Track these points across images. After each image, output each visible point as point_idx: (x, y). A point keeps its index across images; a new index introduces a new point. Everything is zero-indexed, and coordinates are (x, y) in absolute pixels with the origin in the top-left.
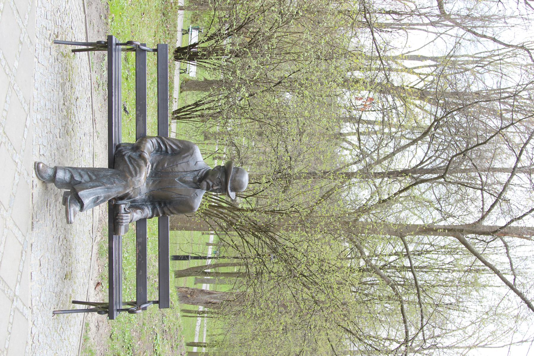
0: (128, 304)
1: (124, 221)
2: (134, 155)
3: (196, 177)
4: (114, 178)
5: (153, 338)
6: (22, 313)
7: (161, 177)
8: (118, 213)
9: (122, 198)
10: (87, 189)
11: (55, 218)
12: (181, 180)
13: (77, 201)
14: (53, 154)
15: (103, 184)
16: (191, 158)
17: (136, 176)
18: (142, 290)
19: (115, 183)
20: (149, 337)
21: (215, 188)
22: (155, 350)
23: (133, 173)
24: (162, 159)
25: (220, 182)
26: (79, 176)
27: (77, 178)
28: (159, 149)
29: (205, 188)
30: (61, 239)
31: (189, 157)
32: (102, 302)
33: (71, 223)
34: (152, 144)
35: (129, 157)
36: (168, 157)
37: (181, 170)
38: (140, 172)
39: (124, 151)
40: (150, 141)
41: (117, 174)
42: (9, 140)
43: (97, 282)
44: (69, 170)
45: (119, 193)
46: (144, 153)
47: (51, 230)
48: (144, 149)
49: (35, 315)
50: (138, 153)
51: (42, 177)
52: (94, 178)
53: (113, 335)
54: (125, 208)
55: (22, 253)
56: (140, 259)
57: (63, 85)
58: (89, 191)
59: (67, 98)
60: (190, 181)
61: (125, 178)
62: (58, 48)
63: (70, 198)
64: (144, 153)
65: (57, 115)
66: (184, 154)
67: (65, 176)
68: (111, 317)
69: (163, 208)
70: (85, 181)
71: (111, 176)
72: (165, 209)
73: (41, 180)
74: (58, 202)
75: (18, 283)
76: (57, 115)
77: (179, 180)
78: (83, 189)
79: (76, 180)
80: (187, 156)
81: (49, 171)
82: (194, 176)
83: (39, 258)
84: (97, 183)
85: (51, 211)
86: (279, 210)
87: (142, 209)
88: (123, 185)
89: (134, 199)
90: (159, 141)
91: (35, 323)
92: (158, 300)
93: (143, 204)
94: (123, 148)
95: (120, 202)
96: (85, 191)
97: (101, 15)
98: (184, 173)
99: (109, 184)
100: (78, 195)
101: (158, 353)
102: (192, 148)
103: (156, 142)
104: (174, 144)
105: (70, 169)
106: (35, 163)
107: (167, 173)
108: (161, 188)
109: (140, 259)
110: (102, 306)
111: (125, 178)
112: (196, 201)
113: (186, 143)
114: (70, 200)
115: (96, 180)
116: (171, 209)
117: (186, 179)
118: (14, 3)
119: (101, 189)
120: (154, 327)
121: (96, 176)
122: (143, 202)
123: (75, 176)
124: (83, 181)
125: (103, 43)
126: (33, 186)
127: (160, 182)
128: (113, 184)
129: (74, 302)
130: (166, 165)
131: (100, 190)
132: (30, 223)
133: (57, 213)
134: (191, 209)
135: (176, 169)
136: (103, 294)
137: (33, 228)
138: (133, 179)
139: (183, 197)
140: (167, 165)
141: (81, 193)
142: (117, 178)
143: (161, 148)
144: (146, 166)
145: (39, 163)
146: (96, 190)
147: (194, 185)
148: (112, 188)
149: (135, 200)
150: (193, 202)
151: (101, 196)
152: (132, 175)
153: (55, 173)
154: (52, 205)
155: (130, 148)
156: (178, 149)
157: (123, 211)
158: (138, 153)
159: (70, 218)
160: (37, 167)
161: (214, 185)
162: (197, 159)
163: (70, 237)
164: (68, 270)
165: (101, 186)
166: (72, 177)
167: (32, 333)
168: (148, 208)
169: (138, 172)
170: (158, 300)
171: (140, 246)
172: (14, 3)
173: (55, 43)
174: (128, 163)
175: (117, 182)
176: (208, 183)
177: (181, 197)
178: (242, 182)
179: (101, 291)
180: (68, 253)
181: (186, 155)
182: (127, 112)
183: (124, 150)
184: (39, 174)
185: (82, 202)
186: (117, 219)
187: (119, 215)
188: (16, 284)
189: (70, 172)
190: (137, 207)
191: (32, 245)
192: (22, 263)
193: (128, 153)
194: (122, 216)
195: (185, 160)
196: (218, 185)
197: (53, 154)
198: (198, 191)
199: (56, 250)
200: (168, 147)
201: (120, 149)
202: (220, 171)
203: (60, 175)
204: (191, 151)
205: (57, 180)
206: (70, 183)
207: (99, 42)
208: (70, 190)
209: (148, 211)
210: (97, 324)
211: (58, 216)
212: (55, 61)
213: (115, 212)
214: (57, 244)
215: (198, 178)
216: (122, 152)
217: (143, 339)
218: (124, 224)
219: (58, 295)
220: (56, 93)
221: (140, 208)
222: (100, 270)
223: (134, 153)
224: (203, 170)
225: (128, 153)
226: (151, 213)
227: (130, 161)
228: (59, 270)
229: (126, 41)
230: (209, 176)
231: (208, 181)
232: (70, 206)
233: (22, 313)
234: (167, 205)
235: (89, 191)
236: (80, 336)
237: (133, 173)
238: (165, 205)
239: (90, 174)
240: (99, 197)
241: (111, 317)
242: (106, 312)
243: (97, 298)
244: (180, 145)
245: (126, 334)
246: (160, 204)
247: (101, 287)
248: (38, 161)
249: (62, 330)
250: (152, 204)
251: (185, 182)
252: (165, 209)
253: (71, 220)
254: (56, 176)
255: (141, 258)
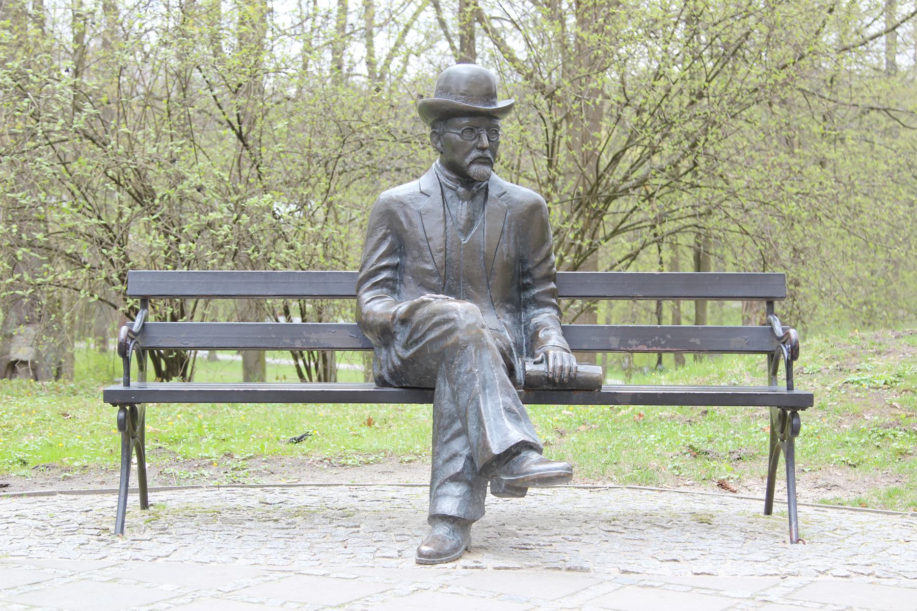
0: (774, 372)
1: (567, 365)
2: (401, 336)
3: (458, 195)
4: (459, 373)
5: (857, 390)
6: (796, 589)
7: (458, 280)
8: (548, 379)
9: (511, 371)
10: (484, 435)
11: (558, 538)
12: (466, 231)
13: (515, 459)
14: (398, 538)
15: (474, 399)
16: (412, 206)
17: (453, 320)
18: (739, 339)
19: (471, 371)
20: (853, 397)
21: (486, 143)
22: (886, 386)
23: (445, 327)
24: (413, 277)
25: (472, 130)
26: (454, 463)
27: (459, 465)
28: (388, 287)
29: (487, 169)
30: (611, 528)
31: (408, 211)
32: (766, 481)
33: (570, 469)
34: (377, 301)
35: (406, 346)
36: (409, 263)
37: (441, 229)
38: (444, 312)
39: (393, 363)
40: (369, 304)
41: (447, 368)
42: (359, 600)
43: (717, 489)
44: (438, 487)
45: (496, 361)
46: (398, 313)
47: (587, 544)
48: (388, 314)
49: (802, 570)
50: (398, 328)
51: (455, 549)
52: (457, 426)
53: (850, 462)
54: (535, 363)
55: (645, 586)
56: (663, 342)
57: (225, 520)
58: (491, 431)
59: (261, 516)
60: (468, 207)
61: (458, 347)
62: (135, 529)
63: (507, 476)
64: (398, 313)
65: (302, 532)
66: (401, 223)
67: (452, 496)
68: (806, 401)
69: (534, 279)
70: (465, 447)
71: (452, 381)
72: (539, 273)
73: (463, 553)
74: (518, 532)
75: (721, 593)
76: (302, 532)
77: (466, 235)
78: (485, 442)
79: (463, 469)
80: (406, 216)
81: (441, 532)
82: (456, 199)
83: (658, 563)
84: (471, 415)
85: (542, 543)
86: (547, 145)
87: (537, 327)
88: (476, 351)
89: (512, 345)
90: (368, 284)
91: (822, 570)
92: (764, 357)
93: (526, 328)
94: (385, 370)
95: (520, 376)
96: (489, 439)
97: (61, 477)
98: (449, 224)
99: (474, 385)
100: (499, 456)
101: (893, 378)
102: (386, 205)
103: (372, 292)
104: (376, 248)
105: (437, 484)
106: (419, 563)
107: (447, 262)
108: (485, 280)
109: (663, 342)
110: (779, 434)
111: (458, 347)
112: (517, 197)
113: (376, 218)
114: (512, 474)
115: (464, 419)
116: (538, 259)
117: (463, 217)
118: (13, 588)
119: (485, 403)
120: (829, 388)
121: (453, 422)
122: (520, 328)
123: (452, 472)
124: (466, 452)
125: (122, 414)
126: (477, 567)
127: (470, 281)
128: (474, 375)
129: (768, 511)
130: (429, 267)
131: (489, 404)
132: (569, 573)
133: (546, 533)
134: (536, 208)
135: (437, 242)
136: (748, 478)
137: (582, 569)
138: (462, 326)
139: (509, 227)
140: (428, 263)
141: (496, 448)
142: (460, 365)
143: (386, 279)
144: (429, 302)
145: (420, 554)
146: (487, 413)
147: (480, 198)
148: (484, 376)
149: (515, 344)
150: (519, 202)
151: (504, 403)
152: (450, 332)
153: (445, 518)
154: (526, 541)
155: (384, 352)
156: (390, 238)
157: (542, 368)
158: (398, 328)
159: (557, 469)
160: (426, 559)
161: (479, 145)
162: (413, 194)
163: (610, 515)
164: (688, 519)
165: (478, 403)
166: (455, 478)
167: (846, 577)
168: (533, 316)
169: (445, 316)
170: (764, 357)
171: (630, 342)
172: (13, 588)
173: (122, 532)
174: (421, 345)
175: (469, 366)
176: (473, 162)
177: (509, 232)
178: (471, 76)
179: (739, 481)
180: (645, 518)
181: (403, 219)
182: (302, 437)
183: (390, 365)
184: (447, 554)
185: (517, 445)
186: (561, 380)
187: (551, 376)
188: (722, 596)
189: (442, 484)
190: (532, 341)
191: (625, 572)
192: (671, 587)
193: (396, 352)
194: (554, 368)
195: (416, 220)
196: (479, 136)
197: (398, 538)
198: (493, 192)
199: (638, 537)
200: (384, 263)
201: (387, 377)
202: (444, 132)
203: (449, 506)
204: (394, 207)
205: (462, 514)
206: (470, 484)
207: (121, 425)
208: (489, 483)
209: (544, 317)
210: (822, 489)
211: (553, 532)
212: (167, 533)
213: (545, 387)
214: (623, 535)
215: (461, 190)
216: (394, 367)
217: (858, 409)
218: (575, 364)
219: (749, 535)
220: (246, 532)
221: (536, 333)
222: (687, 483)
223: (398, 337)
224: (441, 177)
225: (396, 352)
226: (547, 309)
227: (416, 342)
228: (688, 534)
229: (120, 360)
230: (457, 157)
231: (468, 161)
232: (524, 474)
233: (796, 589)
234: (528, 270)
235: (491, 431)
236: (851, 512)
237: (445, 327)
238: (527, 274)
239: (448, 437)
240: (505, 408)
241: (806, 401)
242: (794, 414)
243: (757, 488)
244: (380, 235)
245: (847, 439)
246: (526, 288)
247: (731, 481)
248: (414, 557)
249: (838, 531)
250: (525, 307)
251: (471, 222)
252: (539, 273)
253: (562, 468)
254: (451, 517)
255: (659, 341)
